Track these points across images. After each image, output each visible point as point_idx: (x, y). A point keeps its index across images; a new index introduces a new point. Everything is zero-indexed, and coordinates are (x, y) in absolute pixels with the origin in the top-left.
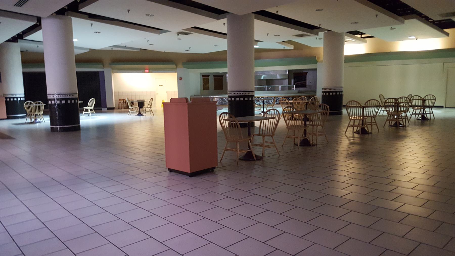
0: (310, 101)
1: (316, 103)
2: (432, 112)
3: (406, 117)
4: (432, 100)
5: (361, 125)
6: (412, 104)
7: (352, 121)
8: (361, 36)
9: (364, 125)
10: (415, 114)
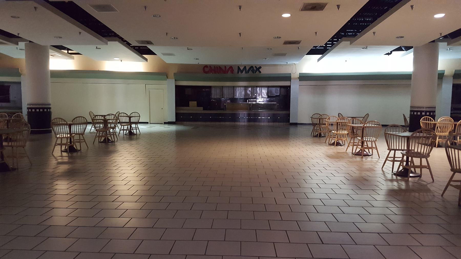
0: (13, 118)
2: (138, 128)
3: (114, 133)
4: (137, 117)
5: (69, 143)
6: (119, 121)
7: (58, 139)
8: (68, 52)
9: (72, 143)
10: (124, 130)
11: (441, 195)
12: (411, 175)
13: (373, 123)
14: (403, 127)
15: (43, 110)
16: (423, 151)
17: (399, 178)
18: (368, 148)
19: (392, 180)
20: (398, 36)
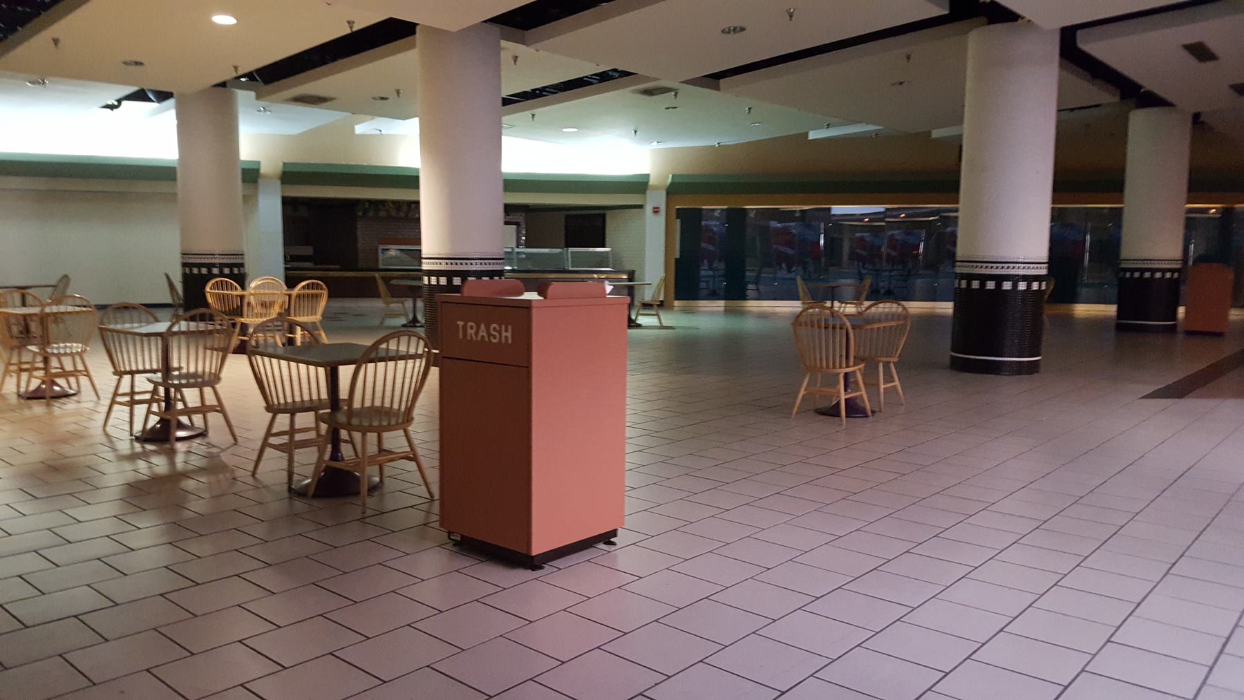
11: (251, 473)
12: (180, 434)
13: (70, 301)
14: (147, 309)
17: (150, 447)
18: (65, 374)
19: (133, 457)
20: (128, 59)
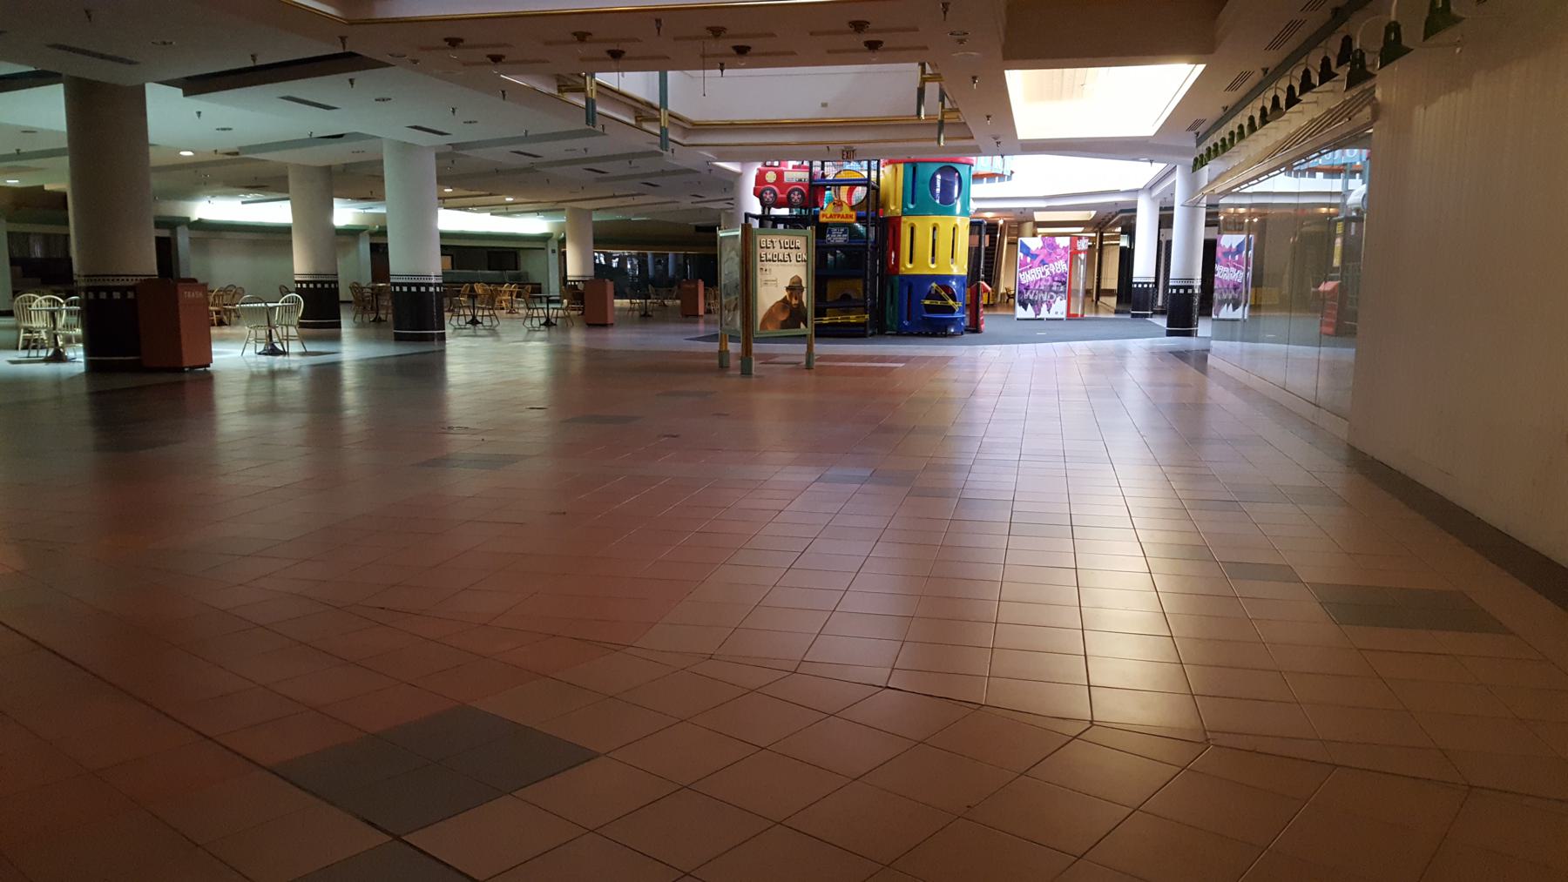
1: (530, 291)
15: (418, 289)
16: (737, 275)
